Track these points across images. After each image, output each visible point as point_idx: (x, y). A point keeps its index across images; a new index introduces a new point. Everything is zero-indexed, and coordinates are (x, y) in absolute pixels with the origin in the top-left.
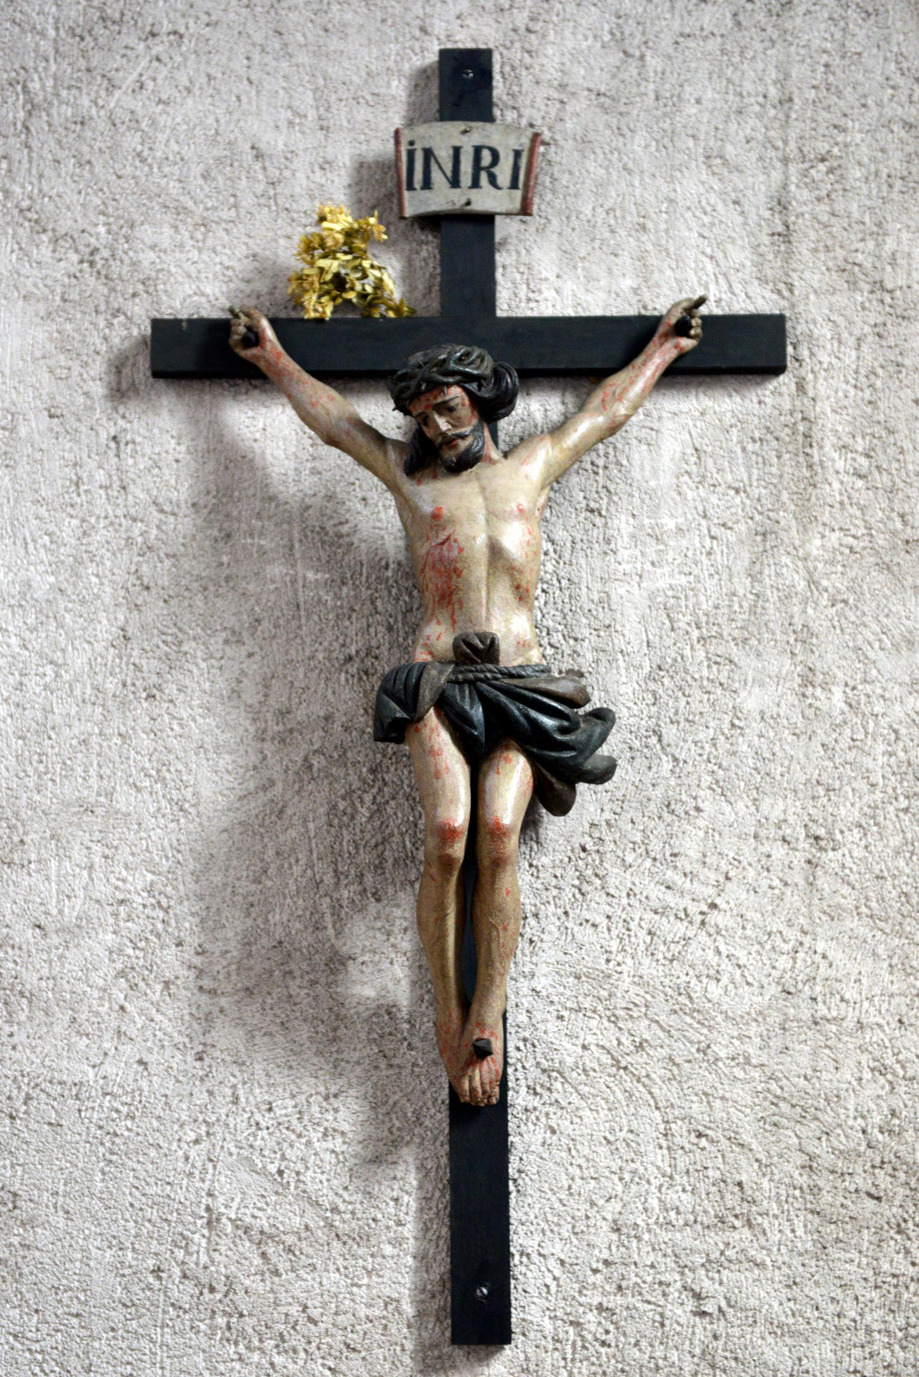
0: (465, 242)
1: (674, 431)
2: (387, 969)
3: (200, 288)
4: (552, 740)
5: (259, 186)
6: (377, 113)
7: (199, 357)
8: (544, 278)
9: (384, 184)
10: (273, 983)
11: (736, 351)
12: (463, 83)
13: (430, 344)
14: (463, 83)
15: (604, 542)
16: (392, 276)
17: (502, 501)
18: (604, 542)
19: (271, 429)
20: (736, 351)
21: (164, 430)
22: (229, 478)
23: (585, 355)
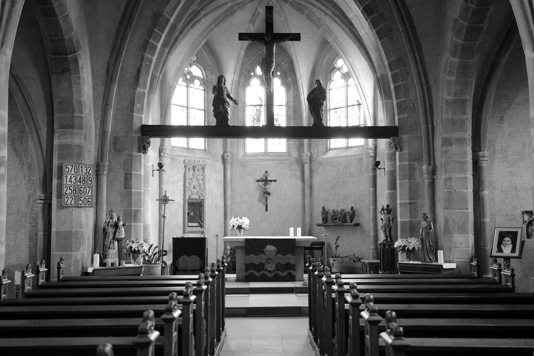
0: (267, 177)
1: (273, 183)
2: (264, 200)
3: (258, 179)
4: (269, 194)
5: (260, 176)
6: (264, 173)
7: (258, 181)
8: (269, 179)
9: (264, 175)
10: (261, 201)
11: (275, 181)
12: (266, 172)
13: (266, 181)
14: (266, 172)
15: (271, 187)
16: (264, 178)
17: (268, 187)
18: (271, 187)
19: (260, 183)
20: (275, 181)
21: (257, 183)
22: (259, 185)
23: (271, 181)
